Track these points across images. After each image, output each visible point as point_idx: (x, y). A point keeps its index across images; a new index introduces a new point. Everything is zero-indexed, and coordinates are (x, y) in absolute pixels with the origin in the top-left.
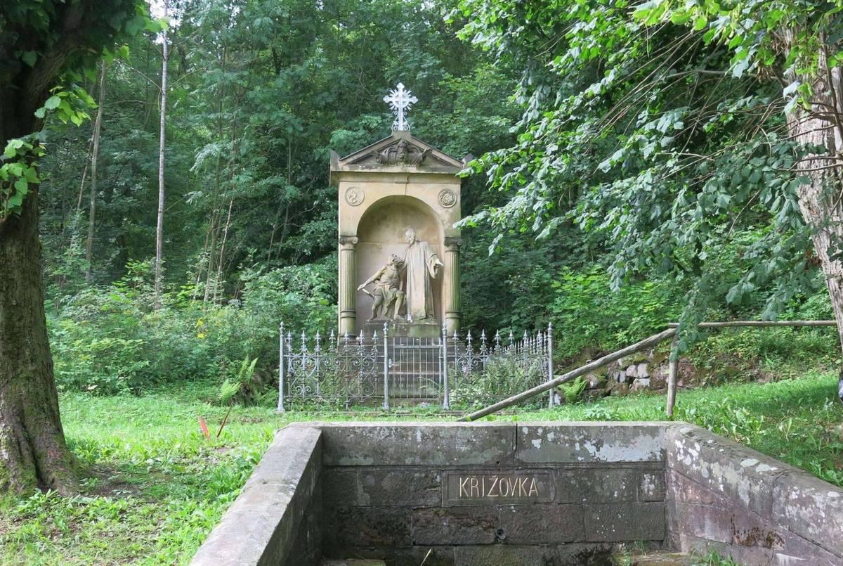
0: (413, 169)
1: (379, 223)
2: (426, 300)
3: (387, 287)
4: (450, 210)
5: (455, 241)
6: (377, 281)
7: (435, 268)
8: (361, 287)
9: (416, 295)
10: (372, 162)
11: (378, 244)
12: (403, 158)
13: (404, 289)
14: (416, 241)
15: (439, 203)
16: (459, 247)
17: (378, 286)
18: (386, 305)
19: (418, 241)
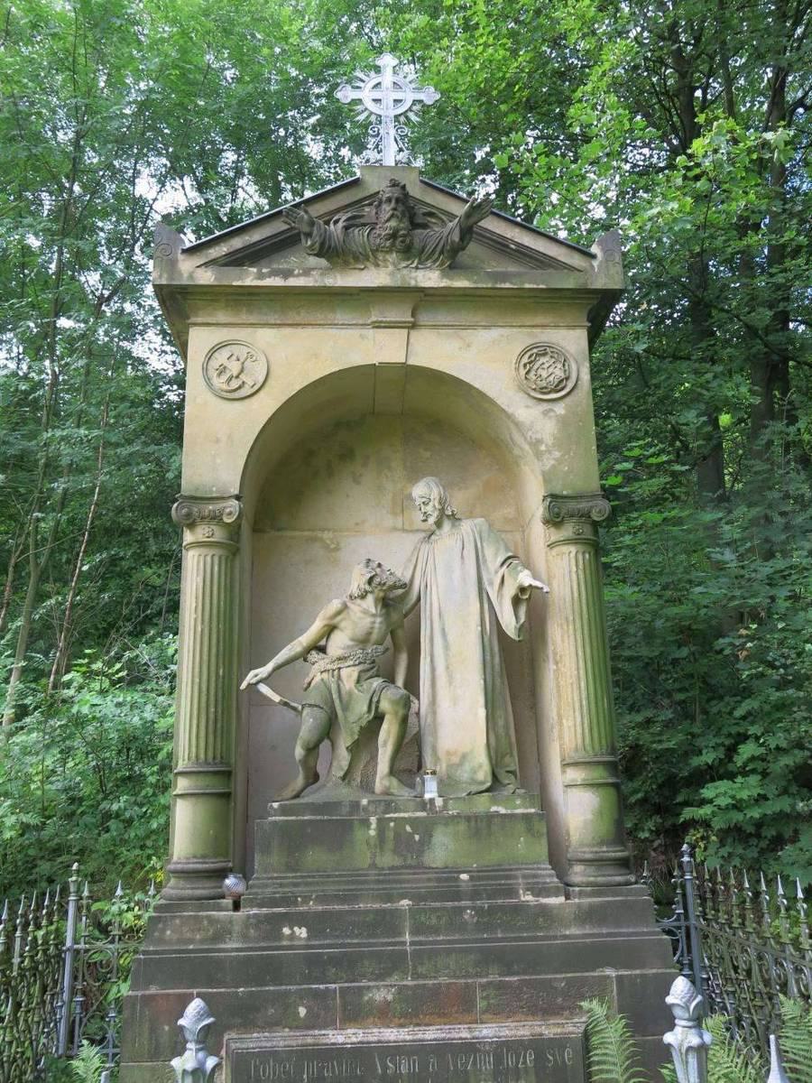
0: (430, 278)
1: (330, 472)
2: (490, 719)
3: (349, 675)
4: (560, 409)
5: (583, 505)
6: (314, 656)
7: (516, 601)
8: (251, 677)
9: (455, 701)
10: (293, 260)
11: (326, 535)
12: (394, 236)
13: (412, 684)
14: (446, 516)
15: (521, 389)
16: (595, 525)
17: (318, 671)
18: (344, 741)
19: (454, 518)
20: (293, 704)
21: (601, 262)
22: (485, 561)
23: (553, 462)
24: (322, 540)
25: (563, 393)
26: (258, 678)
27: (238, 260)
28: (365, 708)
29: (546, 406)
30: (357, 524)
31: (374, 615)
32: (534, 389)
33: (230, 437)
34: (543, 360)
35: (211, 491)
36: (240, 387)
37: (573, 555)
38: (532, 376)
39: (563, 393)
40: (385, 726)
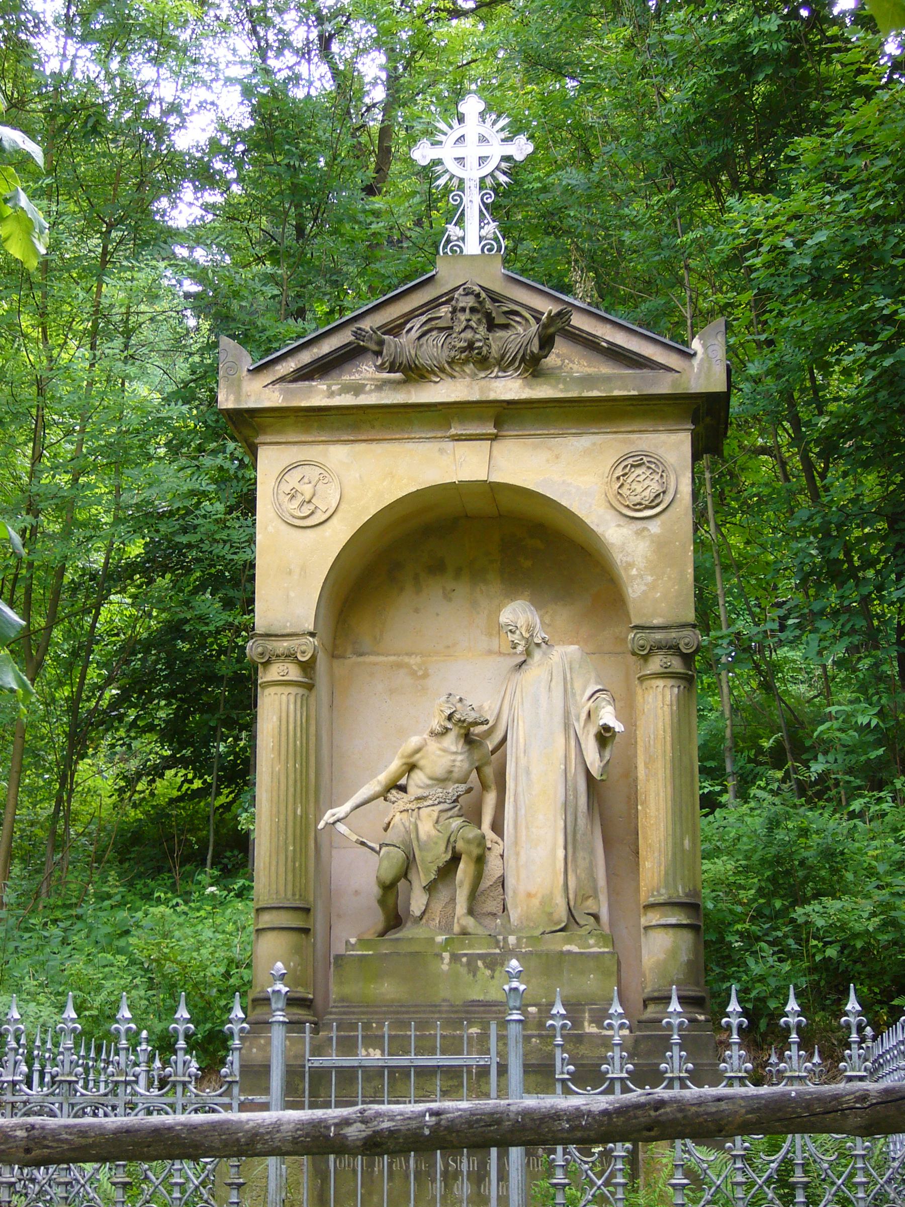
4: (654, 527)
6: (394, 794)
8: (328, 817)
10: (366, 371)
20: (369, 844)
21: (702, 360)
22: (574, 695)
23: (643, 588)
24: (407, 666)
25: (658, 509)
26: (335, 818)
27: (306, 374)
28: (443, 848)
29: (640, 525)
30: (448, 647)
31: (456, 753)
32: (628, 506)
33: (303, 569)
34: (639, 471)
35: (285, 627)
36: (312, 513)
37: (660, 689)
38: (625, 491)
39: (658, 509)
40: (462, 865)
